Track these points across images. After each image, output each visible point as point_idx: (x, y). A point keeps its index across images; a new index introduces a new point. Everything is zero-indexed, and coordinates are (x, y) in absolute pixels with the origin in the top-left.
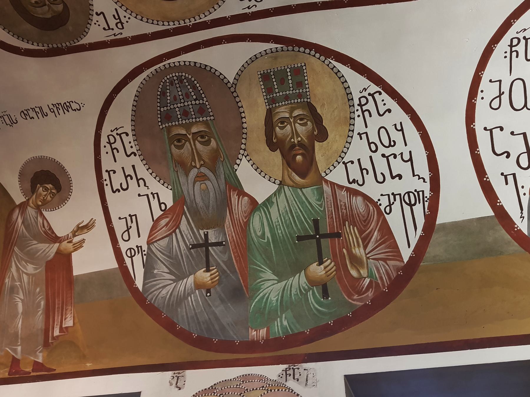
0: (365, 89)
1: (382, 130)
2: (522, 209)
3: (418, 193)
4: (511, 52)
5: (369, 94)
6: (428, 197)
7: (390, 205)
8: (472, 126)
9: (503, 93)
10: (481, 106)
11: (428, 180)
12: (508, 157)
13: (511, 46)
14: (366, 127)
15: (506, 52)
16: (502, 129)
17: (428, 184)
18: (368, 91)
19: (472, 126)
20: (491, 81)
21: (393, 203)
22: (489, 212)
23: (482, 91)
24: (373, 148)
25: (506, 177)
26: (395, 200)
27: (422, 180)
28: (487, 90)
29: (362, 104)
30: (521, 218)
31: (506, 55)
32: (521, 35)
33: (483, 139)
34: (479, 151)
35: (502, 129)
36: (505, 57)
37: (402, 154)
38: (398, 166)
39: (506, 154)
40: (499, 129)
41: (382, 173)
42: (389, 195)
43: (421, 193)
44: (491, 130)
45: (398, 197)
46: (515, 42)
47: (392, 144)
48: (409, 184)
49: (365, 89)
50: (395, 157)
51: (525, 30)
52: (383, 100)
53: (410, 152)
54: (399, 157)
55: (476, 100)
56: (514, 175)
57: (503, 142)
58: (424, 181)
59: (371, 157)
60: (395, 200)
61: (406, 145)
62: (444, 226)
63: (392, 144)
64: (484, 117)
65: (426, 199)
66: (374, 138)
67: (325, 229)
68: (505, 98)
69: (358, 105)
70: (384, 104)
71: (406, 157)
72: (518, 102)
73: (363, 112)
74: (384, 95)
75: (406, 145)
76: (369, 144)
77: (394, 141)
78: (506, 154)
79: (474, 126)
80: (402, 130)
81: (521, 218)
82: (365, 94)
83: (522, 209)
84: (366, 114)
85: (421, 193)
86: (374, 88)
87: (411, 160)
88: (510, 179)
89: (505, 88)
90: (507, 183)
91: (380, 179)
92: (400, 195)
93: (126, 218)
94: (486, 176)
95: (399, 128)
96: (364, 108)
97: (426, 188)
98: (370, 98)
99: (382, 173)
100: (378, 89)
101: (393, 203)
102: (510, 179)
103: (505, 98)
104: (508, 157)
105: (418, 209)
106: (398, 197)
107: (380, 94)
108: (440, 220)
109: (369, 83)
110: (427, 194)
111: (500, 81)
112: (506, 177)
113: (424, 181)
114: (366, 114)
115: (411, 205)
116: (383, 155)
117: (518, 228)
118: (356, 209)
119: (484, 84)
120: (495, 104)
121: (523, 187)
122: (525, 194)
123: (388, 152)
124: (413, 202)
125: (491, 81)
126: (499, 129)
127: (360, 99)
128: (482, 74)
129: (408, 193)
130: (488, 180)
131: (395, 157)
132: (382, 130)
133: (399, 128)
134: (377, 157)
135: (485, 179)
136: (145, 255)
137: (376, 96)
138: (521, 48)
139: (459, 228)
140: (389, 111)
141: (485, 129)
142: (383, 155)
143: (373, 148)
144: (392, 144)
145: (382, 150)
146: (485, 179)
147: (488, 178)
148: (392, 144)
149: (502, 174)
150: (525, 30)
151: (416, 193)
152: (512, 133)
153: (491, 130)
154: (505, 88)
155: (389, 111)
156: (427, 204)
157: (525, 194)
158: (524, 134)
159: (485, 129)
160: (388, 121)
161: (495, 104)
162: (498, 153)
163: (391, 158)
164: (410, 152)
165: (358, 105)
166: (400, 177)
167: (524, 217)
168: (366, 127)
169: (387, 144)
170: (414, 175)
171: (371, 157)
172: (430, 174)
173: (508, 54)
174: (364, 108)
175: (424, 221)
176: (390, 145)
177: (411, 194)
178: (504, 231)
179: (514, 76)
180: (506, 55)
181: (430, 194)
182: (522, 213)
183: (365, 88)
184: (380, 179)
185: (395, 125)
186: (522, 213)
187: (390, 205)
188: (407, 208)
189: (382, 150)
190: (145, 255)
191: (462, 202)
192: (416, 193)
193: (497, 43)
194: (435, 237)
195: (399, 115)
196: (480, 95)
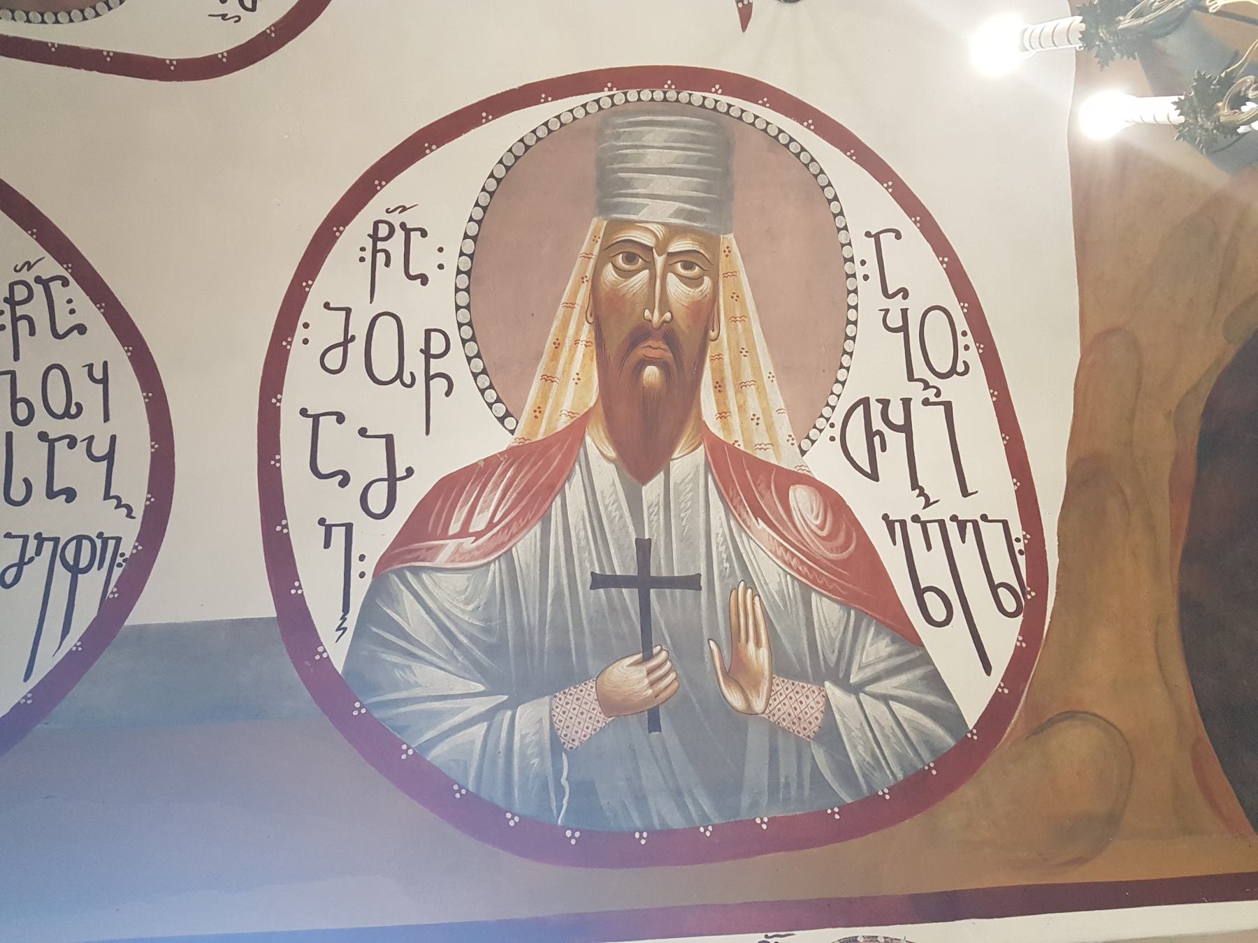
0: (29, 266)
1: (55, 375)
2: (346, 609)
3: (105, 542)
4: (375, 251)
5: (38, 280)
6: (127, 556)
7: (21, 564)
8: (274, 401)
9: (353, 338)
10: (301, 360)
11: (139, 512)
12: (343, 484)
13: (375, 237)
14: (16, 358)
15: (363, 249)
16: (341, 418)
17: (135, 526)
18: (36, 271)
19: (274, 401)
20: (327, 306)
21: (31, 559)
22: (263, 606)
23: (306, 326)
24: (22, 412)
25: (329, 529)
26: (38, 552)
27: (124, 511)
28: (318, 326)
29: (17, 298)
30: (338, 629)
31: (363, 254)
32: (396, 219)
33: (293, 432)
34: (279, 461)
35: (341, 418)
36: (362, 259)
37: (91, 439)
38: (74, 468)
39: (340, 477)
40: (335, 417)
41: (26, 481)
42: (25, 538)
43: (112, 543)
44: (316, 418)
45: (48, 546)
46: (383, 231)
47: (72, 411)
48: (92, 516)
49: (29, 266)
50: (72, 443)
51: (404, 209)
52: (70, 301)
53: (113, 438)
54: (81, 447)
55: (290, 343)
56: (349, 527)
57: (338, 447)
58: (129, 515)
59: (9, 436)
60: (38, 552)
61: (106, 419)
62: (142, 631)
63: (73, 410)
64: (304, 385)
65: (119, 560)
66: (29, 388)
67: (659, 567)
68: (356, 349)
69: (6, 300)
70: (72, 312)
71: (100, 449)
72: (385, 366)
73: (15, 320)
74: (75, 290)
75: (106, 419)
76: (14, 401)
77: (79, 406)
78: (340, 477)
79: (279, 401)
80: (104, 381)
81: (338, 629)
82: (29, 277)
83: (346, 609)
84: (23, 326)
85: (112, 543)
86: (50, 267)
87: (110, 457)
88: (338, 535)
89: (359, 328)
90: (327, 544)
91: (18, 492)
92: (56, 540)
93: (1005, 523)
94: (284, 522)
95: (98, 374)
96: (20, 310)
97: (129, 532)
98: (38, 289)
99: (26, 481)
100: (60, 270)
101: (31, 559)
102: (338, 535)
103: (356, 349)
104: (343, 484)
105: (92, 586)
106: (48, 546)
107: (65, 283)
108: (136, 618)
109: (42, 252)
110: (127, 548)
111: (348, 311)
112: (329, 529)
113: (129, 515)
114: (23, 326)
115: (75, 570)
116: (43, 436)
117: (325, 655)
118: (410, 551)
119: (311, 310)
120: (334, 360)
121: (362, 558)
122: (362, 575)
123: (56, 428)
124: (83, 563)
125: (327, 306)
126: (335, 417)
127: (12, 286)
128: (310, 286)
129: (79, 539)
130: (285, 531)
131: (72, 443)
132: (55, 375)
133: (98, 374)
134: (25, 438)
135: (278, 528)
136: (1021, 552)
137: (55, 286)
138: (395, 246)
139: (187, 642)
140: (81, 329)
141: (304, 412)
142: (43, 436)
143: (22, 412)
144: (73, 410)
145: (42, 421)
146: (278, 528)
147: (286, 526)
148: (72, 411)
149: (322, 522)
150: (404, 209)
151: (99, 543)
152: (363, 432)
153: (316, 418)
154: (359, 328)
155: (81, 329)
156: (117, 572)
157: (362, 575)
158: (389, 439)
159: (304, 412)
160: (73, 354)
161: (334, 360)
162: (323, 471)
163: (61, 446)
164: (113, 438)
165: (6, 300)
166: (70, 494)
167: (345, 629)
168: (16, 358)
169: (59, 408)
170: (107, 496)
171: (9, 436)
172: (148, 499)
173: (368, 255)
174: (20, 310)
175: (95, 614)
176: (67, 414)
177: (86, 544)
178: (287, 660)
179: (379, 306)
180: (363, 254)
181: (135, 547)
182: (344, 619)
183: (28, 263)
184: (18, 492)
185: (91, 366)
186: (344, 619)
187: (21, 564)
188: (62, 577)
189: (42, 421)
190: (1021, 552)
191: (208, 577)
192: (99, 543)
193: (346, 224)
194: (107, 660)
195: (102, 342)
196: (300, 333)
